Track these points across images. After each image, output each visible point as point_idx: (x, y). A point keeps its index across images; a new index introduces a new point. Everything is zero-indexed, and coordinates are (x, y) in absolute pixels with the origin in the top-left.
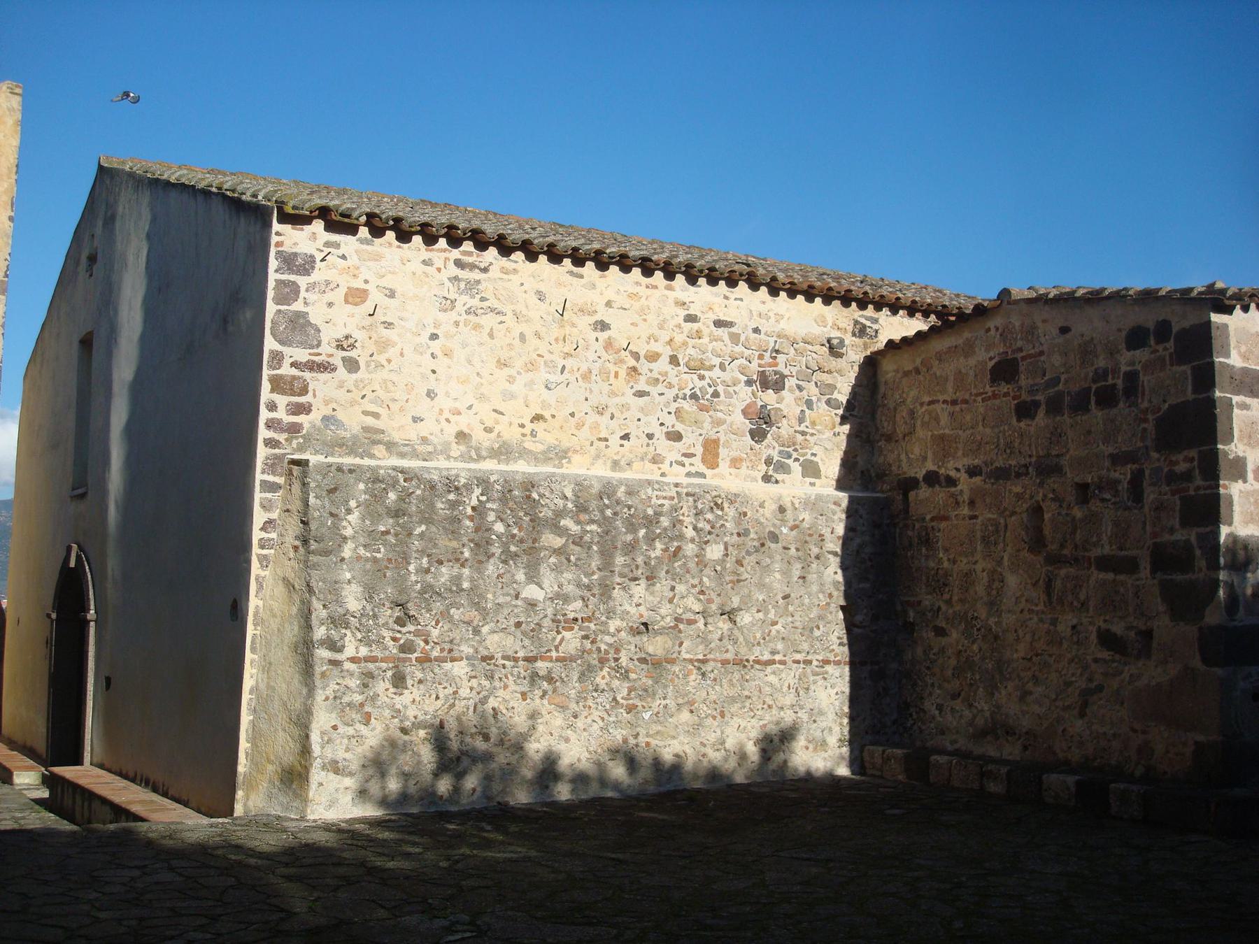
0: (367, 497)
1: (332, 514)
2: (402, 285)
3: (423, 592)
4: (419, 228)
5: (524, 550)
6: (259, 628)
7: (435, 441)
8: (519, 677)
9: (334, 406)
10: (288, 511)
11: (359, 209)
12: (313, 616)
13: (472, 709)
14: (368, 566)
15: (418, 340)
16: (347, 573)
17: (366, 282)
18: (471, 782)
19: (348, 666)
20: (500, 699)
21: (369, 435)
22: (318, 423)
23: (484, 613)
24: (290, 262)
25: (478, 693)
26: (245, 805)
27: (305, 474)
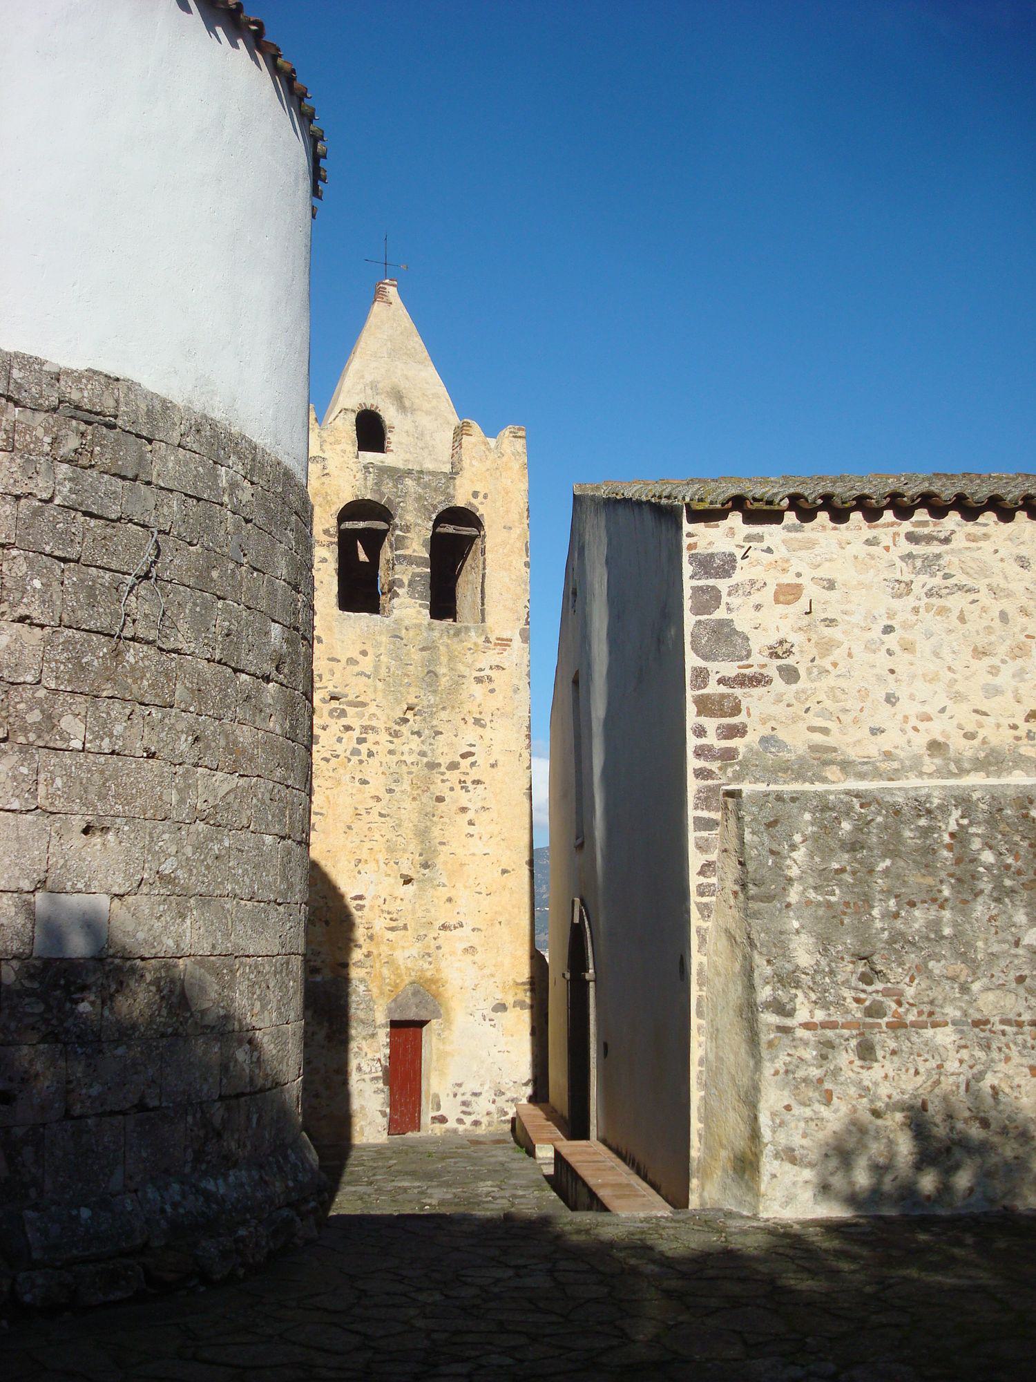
0: (815, 829)
1: (772, 852)
2: (842, 572)
3: (892, 941)
4: (854, 502)
5: (1023, 884)
6: (705, 988)
7: (902, 754)
8: (1025, 1047)
9: (773, 724)
10: (725, 851)
11: (779, 491)
12: (756, 974)
13: (963, 1087)
14: (821, 912)
15: (868, 635)
16: (794, 921)
17: (799, 575)
18: (963, 1180)
19: (801, 1033)
20: (1000, 1075)
21: (818, 755)
22: (756, 746)
23: (973, 966)
24: (706, 565)
25: (971, 1067)
26: (701, 1196)
27: (739, 807)
